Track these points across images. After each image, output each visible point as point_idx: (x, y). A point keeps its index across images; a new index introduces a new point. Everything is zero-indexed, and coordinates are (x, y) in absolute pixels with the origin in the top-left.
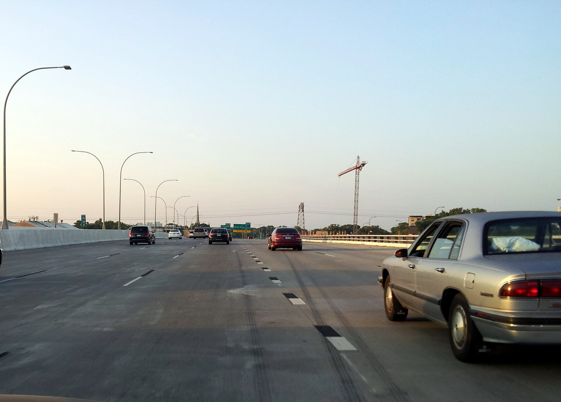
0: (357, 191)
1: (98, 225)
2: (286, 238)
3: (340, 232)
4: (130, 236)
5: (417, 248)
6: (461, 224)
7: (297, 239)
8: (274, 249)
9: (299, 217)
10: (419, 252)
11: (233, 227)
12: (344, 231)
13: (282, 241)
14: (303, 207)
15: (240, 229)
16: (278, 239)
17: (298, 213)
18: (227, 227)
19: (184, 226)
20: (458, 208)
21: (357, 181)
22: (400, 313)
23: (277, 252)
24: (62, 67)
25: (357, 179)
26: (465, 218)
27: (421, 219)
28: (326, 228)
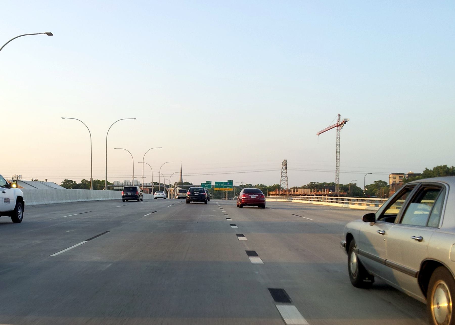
0: (339, 149)
1: (85, 185)
2: (252, 197)
3: (323, 190)
4: (123, 194)
5: (386, 211)
6: (439, 188)
7: (261, 198)
8: (241, 206)
9: (282, 175)
10: (388, 217)
11: (214, 185)
12: (327, 189)
13: (248, 200)
14: (286, 164)
15: (222, 187)
16: (245, 198)
17: (281, 170)
18: (208, 185)
19: (169, 185)
20: (442, 166)
21: (338, 138)
22: (366, 280)
23: (245, 209)
24: (44, 34)
25: (339, 137)
26: (445, 182)
27: (403, 177)
28: (306, 186)
